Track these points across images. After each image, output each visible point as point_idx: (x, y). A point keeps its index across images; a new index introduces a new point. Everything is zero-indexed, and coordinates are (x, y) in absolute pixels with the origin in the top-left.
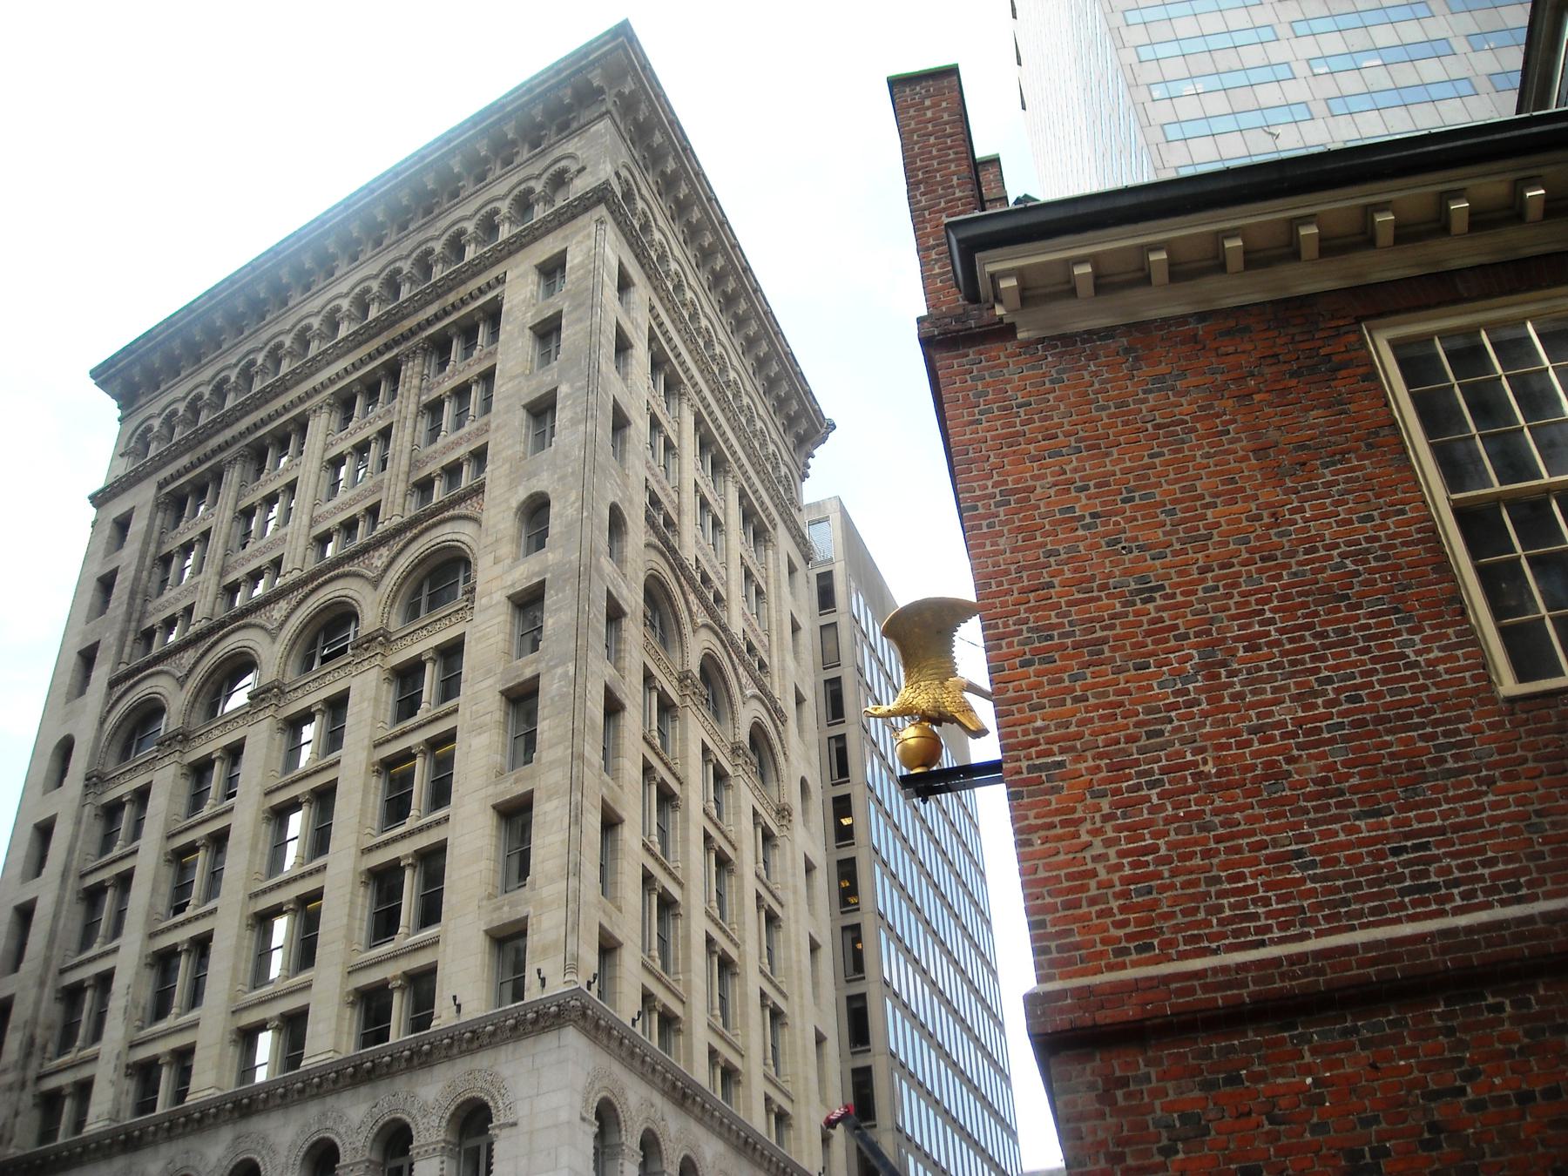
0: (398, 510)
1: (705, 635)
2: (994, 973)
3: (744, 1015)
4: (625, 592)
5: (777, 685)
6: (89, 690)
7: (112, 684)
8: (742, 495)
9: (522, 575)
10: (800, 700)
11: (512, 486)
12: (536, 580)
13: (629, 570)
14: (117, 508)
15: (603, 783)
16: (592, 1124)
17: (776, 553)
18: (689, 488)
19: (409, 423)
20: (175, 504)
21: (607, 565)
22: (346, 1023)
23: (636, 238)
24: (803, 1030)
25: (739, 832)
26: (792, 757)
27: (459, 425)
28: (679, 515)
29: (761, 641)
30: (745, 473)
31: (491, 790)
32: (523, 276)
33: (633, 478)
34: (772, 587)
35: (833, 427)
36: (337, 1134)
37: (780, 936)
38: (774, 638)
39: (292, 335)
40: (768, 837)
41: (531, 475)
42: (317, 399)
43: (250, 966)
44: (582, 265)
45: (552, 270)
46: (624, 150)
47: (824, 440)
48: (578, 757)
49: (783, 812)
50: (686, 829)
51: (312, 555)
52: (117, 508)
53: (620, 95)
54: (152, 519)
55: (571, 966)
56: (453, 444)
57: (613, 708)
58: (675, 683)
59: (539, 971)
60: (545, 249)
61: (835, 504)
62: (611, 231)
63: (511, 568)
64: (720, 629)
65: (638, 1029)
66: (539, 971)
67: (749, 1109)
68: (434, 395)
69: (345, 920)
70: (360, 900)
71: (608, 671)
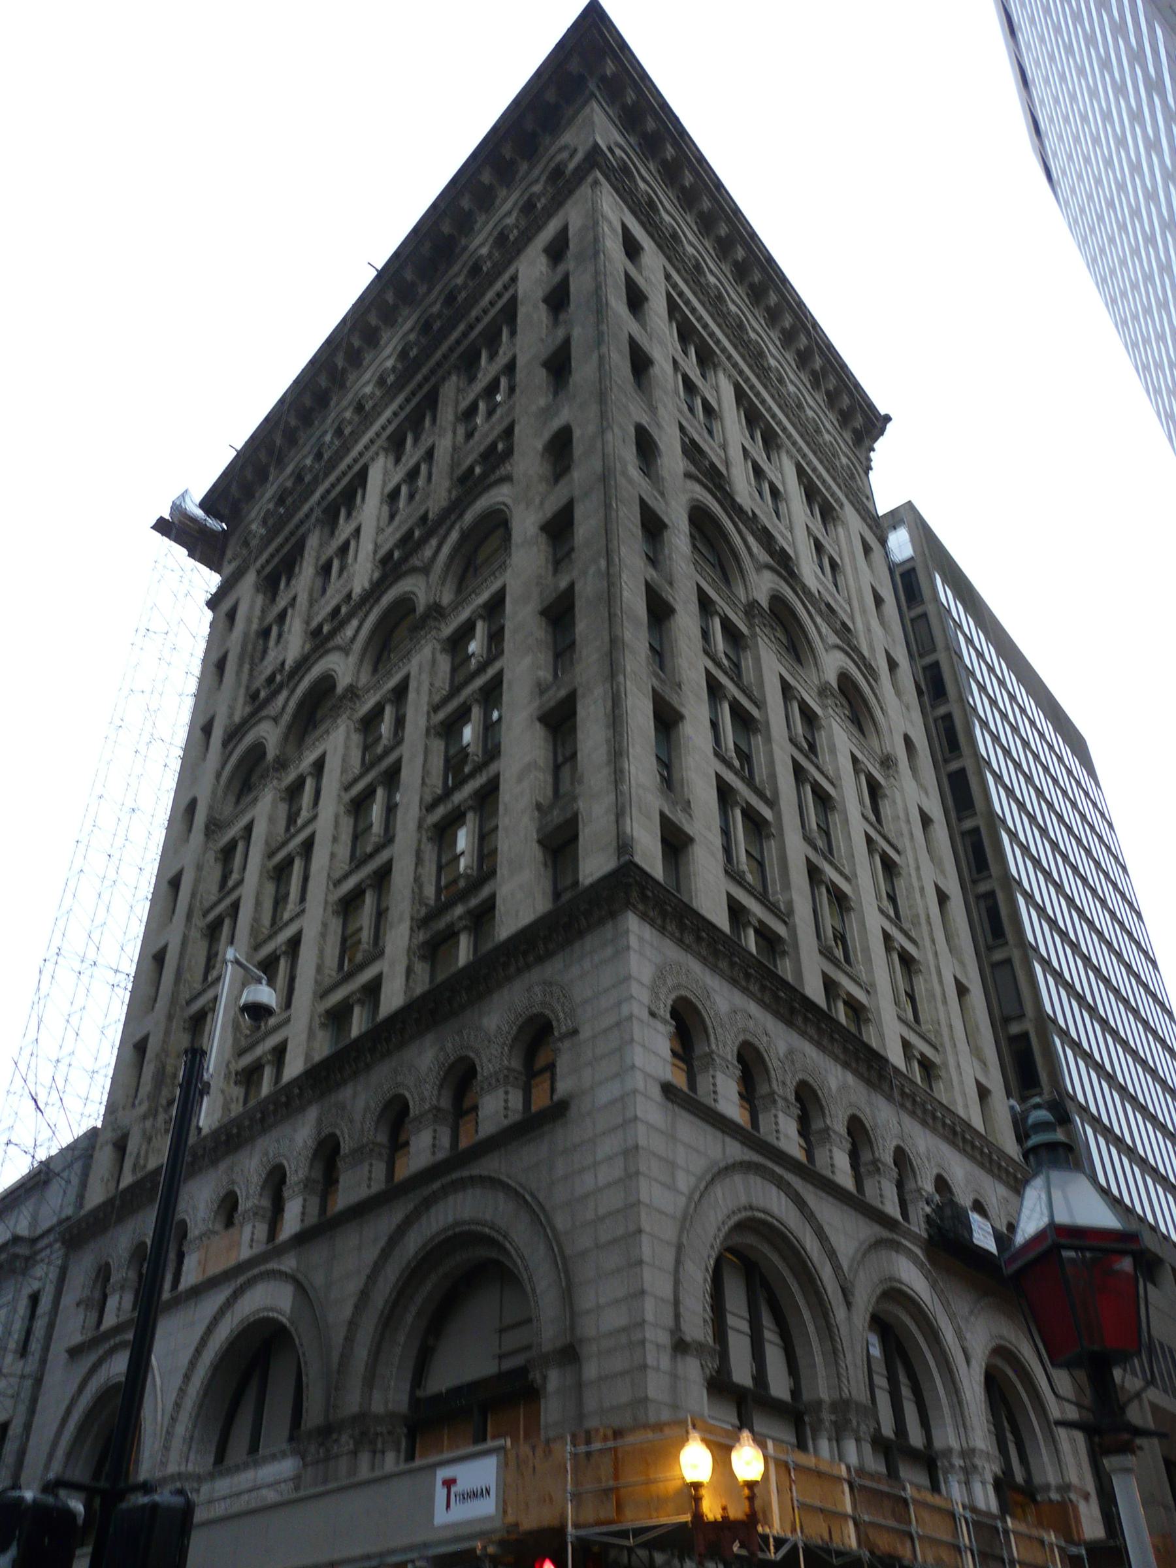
1: (768, 575)
2: (1154, 963)
7: (225, 744)
14: (226, 606)
16: (665, 1022)
18: (735, 454)
23: (645, 210)
25: (837, 769)
26: (890, 712)
28: (727, 469)
35: (887, 419)
37: (901, 884)
40: (874, 789)
42: (374, 448)
45: (557, 251)
47: (882, 432)
49: (887, 762)
52: (226, 606)
53: (603, 78)
54: (253, 602)
56: (486, 428)
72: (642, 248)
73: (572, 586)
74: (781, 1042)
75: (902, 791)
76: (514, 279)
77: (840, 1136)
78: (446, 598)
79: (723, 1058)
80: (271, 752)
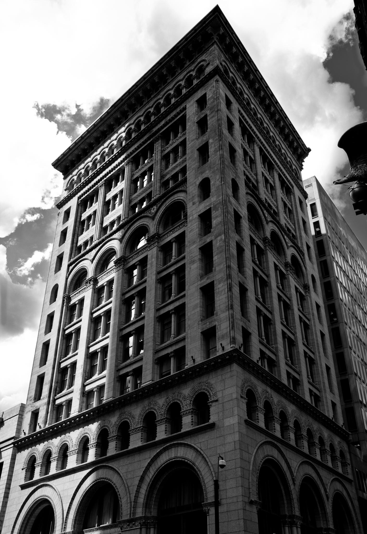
0: (158, 192)
1: (270, 224)
3: (299, 359)
4: (240, 209)
5: (299, 243)
6: (62, 268)
7: (69, 266)
8: (280, 176)
9: (203, 207)
10: (308, 247)
11: (196, 177)
12: (208, 208)
13: (241, 202)
15: (238, 277)
16: (245, 399)
17: (294, 196)
18: (260, 178)
19: (159, 162)
20: (84, 205)
21: (233, 200)
22: (156, 370)
23: (231, 86)
24: (321, 365)
25: (291, 294)
26: (308, 268)
27: (175, 161)
29: (292, 227)
30: (280, 168)
31: (199, 283)
32: (192, 105)
33: (239, 170)
34: (294, 208)
36: (155, 410)
38: (297, 226)
39: (173, 90)
41: (202, 173)
43: (122, 354)
44: (212, 97)
45: (202, 103)
46: (222, 56)
48: (229, 267)
50: (271, 293)
51: (131, 213)
53: (219, 35)
55: (233, 341)
56: (173, 168)
57: (240, 250)
58: (262, 242)
59: (221, 344)
60: (199, 94)
61: (314, 179)
62: (221, 84)
63: (199, 205)
64: (277, 222)
65: (260, 364)
66: (221, 344)
67: (304, 394)
68: (166, 152)
69: (152, 335)
70: (157, 327)
71: (237, 238)
72: (232, 103)
73: (211, 242)
74: (276, 398)
75: (310, 297)
76: (185, 109)
77: (292, 428)
78: (161, 231)
79: (260, 408)
80: (90, 274)
